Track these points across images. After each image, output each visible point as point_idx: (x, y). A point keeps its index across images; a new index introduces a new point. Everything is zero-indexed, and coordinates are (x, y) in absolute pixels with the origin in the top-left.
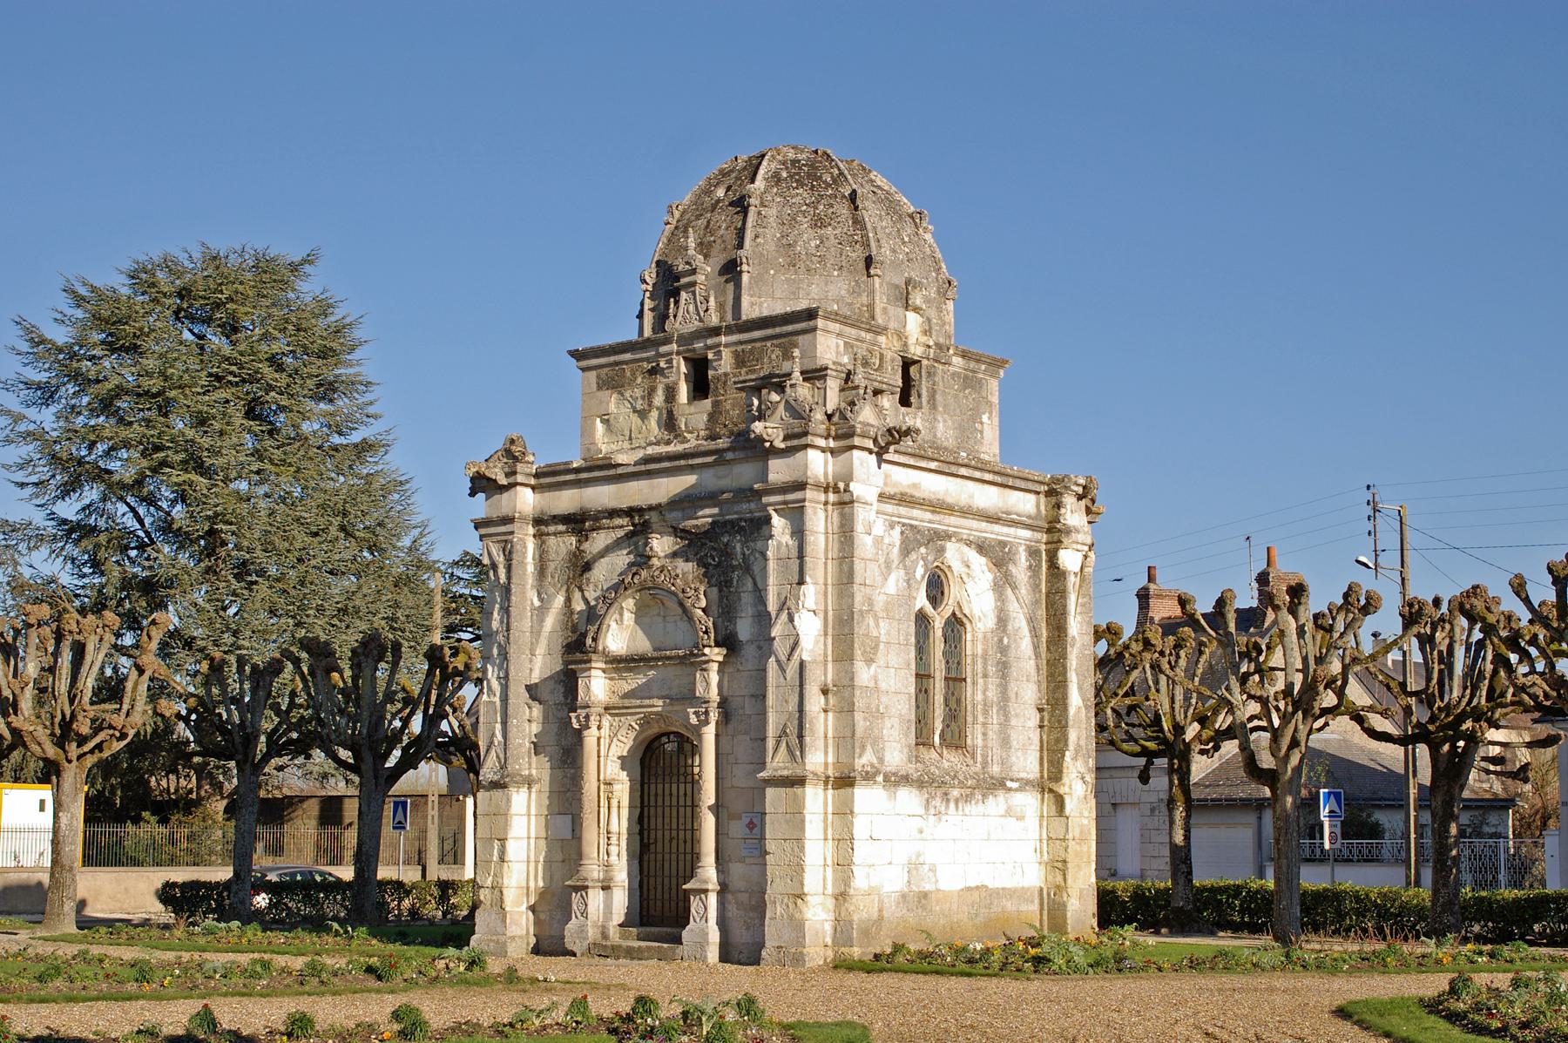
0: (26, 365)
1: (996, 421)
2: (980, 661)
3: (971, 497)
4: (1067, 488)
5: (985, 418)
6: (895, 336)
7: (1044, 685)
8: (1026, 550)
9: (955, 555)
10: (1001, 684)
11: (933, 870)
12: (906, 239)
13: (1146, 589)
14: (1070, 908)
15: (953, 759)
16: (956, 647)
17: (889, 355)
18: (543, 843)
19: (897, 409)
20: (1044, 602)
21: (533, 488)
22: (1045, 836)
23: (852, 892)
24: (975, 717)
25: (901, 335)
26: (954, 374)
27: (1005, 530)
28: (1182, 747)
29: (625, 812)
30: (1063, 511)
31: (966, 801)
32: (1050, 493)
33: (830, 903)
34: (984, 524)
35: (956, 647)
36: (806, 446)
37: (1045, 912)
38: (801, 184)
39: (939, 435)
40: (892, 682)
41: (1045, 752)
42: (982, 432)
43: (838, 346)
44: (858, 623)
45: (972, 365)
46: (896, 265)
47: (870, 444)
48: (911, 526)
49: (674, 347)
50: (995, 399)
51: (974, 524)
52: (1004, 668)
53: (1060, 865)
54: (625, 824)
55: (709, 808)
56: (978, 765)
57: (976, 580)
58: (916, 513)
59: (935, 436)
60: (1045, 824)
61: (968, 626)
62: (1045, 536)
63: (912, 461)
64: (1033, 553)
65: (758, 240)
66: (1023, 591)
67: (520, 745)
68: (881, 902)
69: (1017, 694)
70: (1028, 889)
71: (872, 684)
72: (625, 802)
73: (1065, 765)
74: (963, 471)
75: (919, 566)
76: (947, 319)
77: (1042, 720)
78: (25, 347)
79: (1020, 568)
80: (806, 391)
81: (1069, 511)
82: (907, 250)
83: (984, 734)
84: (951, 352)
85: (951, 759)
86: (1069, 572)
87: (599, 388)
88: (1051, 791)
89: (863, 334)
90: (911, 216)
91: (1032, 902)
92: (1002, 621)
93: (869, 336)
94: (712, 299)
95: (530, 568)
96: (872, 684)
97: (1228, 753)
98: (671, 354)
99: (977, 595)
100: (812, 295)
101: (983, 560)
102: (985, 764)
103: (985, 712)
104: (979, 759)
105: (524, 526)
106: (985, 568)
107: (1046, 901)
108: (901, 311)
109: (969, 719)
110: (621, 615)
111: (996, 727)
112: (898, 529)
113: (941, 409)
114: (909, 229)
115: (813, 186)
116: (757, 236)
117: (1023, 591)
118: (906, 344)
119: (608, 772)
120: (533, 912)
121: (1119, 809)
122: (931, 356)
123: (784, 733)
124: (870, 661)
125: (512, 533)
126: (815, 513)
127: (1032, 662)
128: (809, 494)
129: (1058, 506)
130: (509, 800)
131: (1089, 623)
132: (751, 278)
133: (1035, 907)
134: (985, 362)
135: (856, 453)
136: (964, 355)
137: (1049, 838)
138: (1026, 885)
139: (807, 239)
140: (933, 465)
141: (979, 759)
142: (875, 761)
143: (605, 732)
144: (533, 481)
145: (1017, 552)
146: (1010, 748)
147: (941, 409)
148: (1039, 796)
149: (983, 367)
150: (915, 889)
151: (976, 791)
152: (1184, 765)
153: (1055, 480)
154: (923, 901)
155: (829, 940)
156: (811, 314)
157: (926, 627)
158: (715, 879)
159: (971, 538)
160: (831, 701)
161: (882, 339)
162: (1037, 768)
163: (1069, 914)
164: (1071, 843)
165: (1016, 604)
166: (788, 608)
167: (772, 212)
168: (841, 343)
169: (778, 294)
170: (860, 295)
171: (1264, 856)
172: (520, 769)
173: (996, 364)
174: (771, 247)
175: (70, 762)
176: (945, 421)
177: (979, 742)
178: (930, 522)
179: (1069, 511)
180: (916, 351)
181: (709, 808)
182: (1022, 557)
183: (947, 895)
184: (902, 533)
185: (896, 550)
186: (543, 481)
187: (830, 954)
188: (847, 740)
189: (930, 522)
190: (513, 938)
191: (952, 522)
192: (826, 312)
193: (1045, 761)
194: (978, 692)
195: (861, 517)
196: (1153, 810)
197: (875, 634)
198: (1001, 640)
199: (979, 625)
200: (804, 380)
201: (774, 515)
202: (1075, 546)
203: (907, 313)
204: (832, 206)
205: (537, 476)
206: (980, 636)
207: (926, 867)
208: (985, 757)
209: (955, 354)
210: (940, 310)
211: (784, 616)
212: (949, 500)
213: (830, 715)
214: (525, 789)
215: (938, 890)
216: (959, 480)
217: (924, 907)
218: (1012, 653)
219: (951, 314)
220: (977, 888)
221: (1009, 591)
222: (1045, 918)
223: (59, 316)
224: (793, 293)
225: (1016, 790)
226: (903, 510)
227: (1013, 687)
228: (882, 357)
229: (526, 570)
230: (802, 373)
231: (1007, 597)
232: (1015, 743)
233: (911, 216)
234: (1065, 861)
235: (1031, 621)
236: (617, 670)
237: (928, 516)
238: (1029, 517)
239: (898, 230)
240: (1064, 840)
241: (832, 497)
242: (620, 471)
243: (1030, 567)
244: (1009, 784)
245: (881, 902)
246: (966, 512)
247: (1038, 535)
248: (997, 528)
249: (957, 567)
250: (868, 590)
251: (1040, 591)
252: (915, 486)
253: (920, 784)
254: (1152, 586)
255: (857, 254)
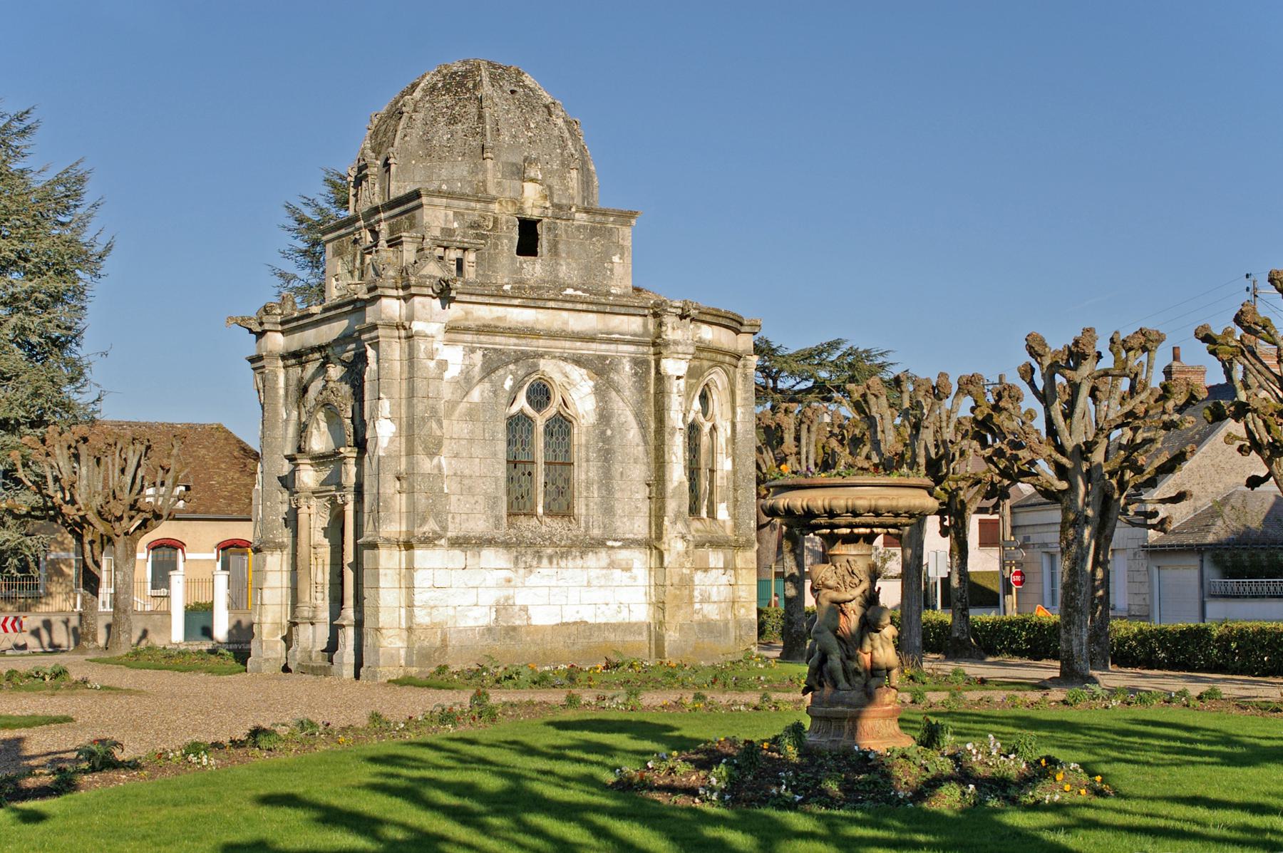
0: (296, 238)
1: (628, 260)
2: (583, 449)
3: (567, 323)
4: (665, 310)
5: (616, 259)
6: (510, 204)
7: (653, 466)
8: (630, 361)
9: (549, 368)
10: (603, 466)
11: (525, 609)
12: (532, 126)
13: (1170, 366)
14: (667, 638)
15: (555, 525)
16: (564, 439)
17: (503, 218)
18: (289, 590)
19: (513, 259)
20: (652, 400)
21: (283, 332)
22: (653, 583)
23: (415, 626)
24: (580, 493)
25: (517, 202)
26: (579, 228)
27: (604, 347)
28: (959, 506)
29: (328, 569)
30: (664, 328)
31: (561, 557)
32: (656, 315)
33: (404, 634)
34: (578, 344)
35: (564, 439)
36: (380, 297)
37: (653, 642)
38: (448, 91)
39: (561, 275)
40: (477, 469)
41: (653, 519)
42: (611, 270)
43: (446, 215)
44: (418, 426)
45: (598, 218)
46: (513, 148)
47: (430, 292)
48: (495, 350)
49: (362, 223)
50: (628, 243)
51: (568, 344)
52: (607, 455)
53: (660, 605)
54: (327, 577)
55: (349, 565)
56: (582, 529)
57: (578, 387)
58: (498, 339)
59: (557, 276)
60: (653, 573)
61: (574, 422)
62: (652, 349)
63: (492, 300)
64: (638, 363)
65: (406, 138)
66: (627, 393)
67: (274, 521)
68: (444, 635)
69: (622, 473)
70: (636, 624)
71: (436, 471)
72: (328, 561)
73: (664, 528)
74: (552, 304)
75: (508, 380)
76: (571, 184)
77: (650, 493)
78: (295, 225)
79: (625, 374)
80: (391, 254)
81: (669, 328)
82: (530, 134)
83: (587, 505)
84: (573, 210)
85: (557, 525)
86: (669, 377)
87: (333, 256)
88: (656, 548)
89: (473, 204)
90: (547, 107)
91: (640, 634)
92: (605, 416)
93: (478, 206)
94: (377, 185)
95: (282, 392)
96: (436, 471)
97: (1204, 505)
98: (361, 228)
99: (581, 398)
100: (443, 177)
101: (584, 371)
102: (587, 528)
103: (588, 488)
104: (583, 525)
105: (275, 361)
106: (586, 377)
107: (653, 634)
108: (517, 183)
109: (576, 494)
110: (318, 424)
111: (597, 500)
112: (479, 354)
113: (564, 255)
114: (540, 116)
115: (457, 92)
116: (405, 136)
117: (627, 393)
118: (521, 208)
119: (316, 539)
120: (285, 641)
121: (1116, 553)
122: (550, 215)
123: (372, 511)
124: (431, 455)
125: (264, 367)
126: (389, 346)
127: (641, 448)
128: (381, 332)
129: (660, 325)
130: (264, 561)
131: (751, 413)
132: (398, 168)
133: (645, 637)
134: (612, 215)
135: (417, 299)
136: (587, 211)
137: (656, 585)
138: (633, 620)
139: (442, 134)
140: (516, 302)
141: (583, 525)
142: (437, 529)
143: (313, 510)
144: (280, 328)
145: (620, 362)
146: (614, 515)
147: (564, 255)
148: (648, 552)
149: (612, 219)
150: (502, 623)
151: (573, 549)
152: (959, 521)
153: (656, 305)
154: (512, 633)
155: (403, 662)
156: (416, 195)
157: (530, 425)
158: (352, 617)
159: (565, 355)
160: (405, 486)
161: (495, 207)
162: (647, 530)
163: (666, 644)
164: (669, 589)
165: (621, 404)
166: (374, 418)
167: (419, 117)
168: (451, 213)
169: (417, 179)
170: (477, 174)
171: (1206, 592)
172: (274, 538)
173: (625, 217)
174: (415, 143)
175: (118, 536)
176: (568, 264)
177: (583, 511)
178: (515, 345)
179: (669, 328)
180: (532, 213)
181: (349, 565)
182: (627, 367)
183: (538, 629)
184: (484, 355)
185: (477, 369)
186: (286, 327)
187: (401, 671)
188: (414, 515)
189: (515, 345)
190: (267, 660)
191: (541, 344)
192: (427, 190)
193: (653, 524)
194: (584, 472)
195: (423, 347)
196: (1135, 554)
197: (438, 433)
198: (603, 432)
199: (583, 421)
200: (389, 246)
201: (368, 348)
202: (675, 356)
203: (525, 184)
204: (465, 106)
205: (282, 323)
206: (584, 429)
207: (517, 609)
208: (587, 523)
209: (577, 211)
210: (562, 178)
211: (372, 423)
212: (539, 327)
213: (404, 496)
214: (279, 552)
215: (529, 625)
216: (550, 311)
217: (512, 638)
218: (616, 443)
219: (575, 181)
220: (575, 623)
221: (613, 394)
222: (653, 646)
223: (305, 201)
224: (429, 177)
225: (620, 548)
226: (483, 338)
227: (617, 468)
228: (496, 221)
229: (278, 393)
230: (387, 242)
231: (610, 398)
232: (620, 512)
233: (547, 107)
234: (663, 602)
235: (638, 415)
236: (318, 465)
237: (513, 340)
238: (635, 335)
239: (526, 119)
240: (663, 586)
241: (403, 333)
242: (315, 318)
243: (636, 374)
244: (609, 543)
245: (444, 635)
246: (552, 335)
247: (645, 349)
248: (593, 346)
249: (557, 378)
250: (431, 401)
251: (648, 392)
252: (499, 318)
253: (507, 545)
254: (1176, 364)
255: (475, 143)
